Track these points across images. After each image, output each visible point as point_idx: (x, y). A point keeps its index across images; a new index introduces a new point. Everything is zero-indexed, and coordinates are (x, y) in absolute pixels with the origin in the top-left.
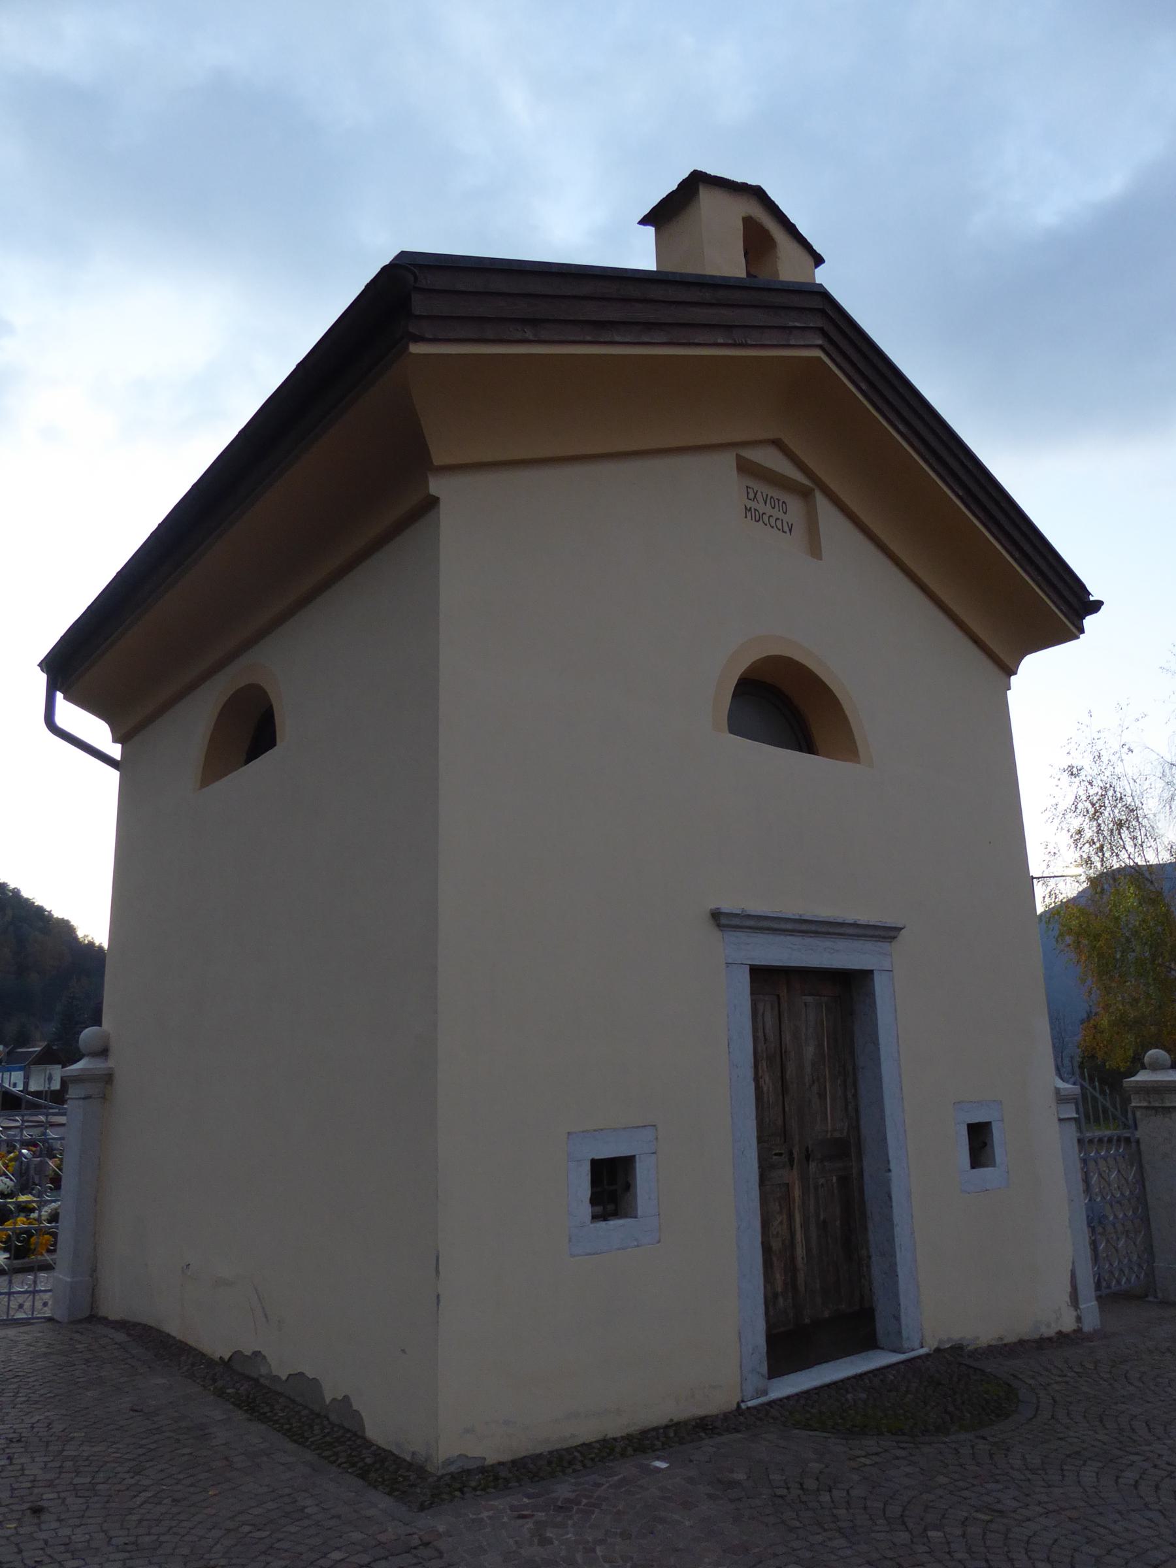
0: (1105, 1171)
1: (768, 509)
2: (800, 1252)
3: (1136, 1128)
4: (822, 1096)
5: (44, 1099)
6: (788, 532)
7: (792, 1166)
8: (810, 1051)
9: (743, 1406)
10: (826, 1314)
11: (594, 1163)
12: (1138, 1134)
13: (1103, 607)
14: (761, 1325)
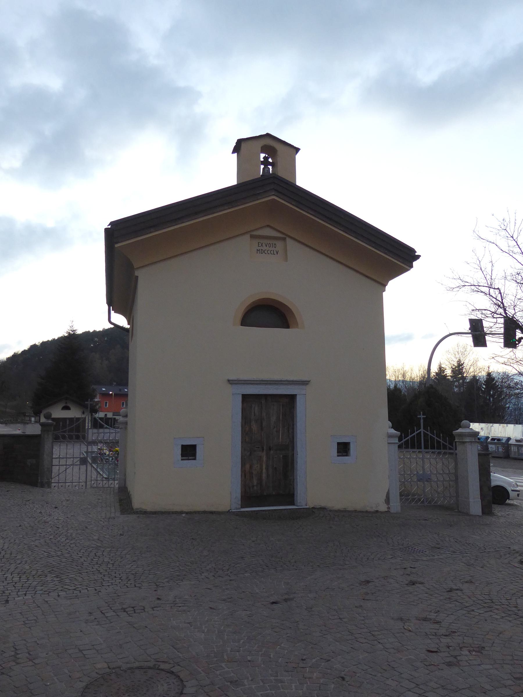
0: (408, 462)
1: (267, 248)
2: (264, 476)
3: (456, 449)
4: (278, 432)
5: (113, 427)
6: (276, 254)
7: (23, 433)
8: (273, 419)
9: (230, 511)
10: (274, 493)
11: (182, 446)
12: (457, 451)
13: (420, 257)
14: (239, 491)
